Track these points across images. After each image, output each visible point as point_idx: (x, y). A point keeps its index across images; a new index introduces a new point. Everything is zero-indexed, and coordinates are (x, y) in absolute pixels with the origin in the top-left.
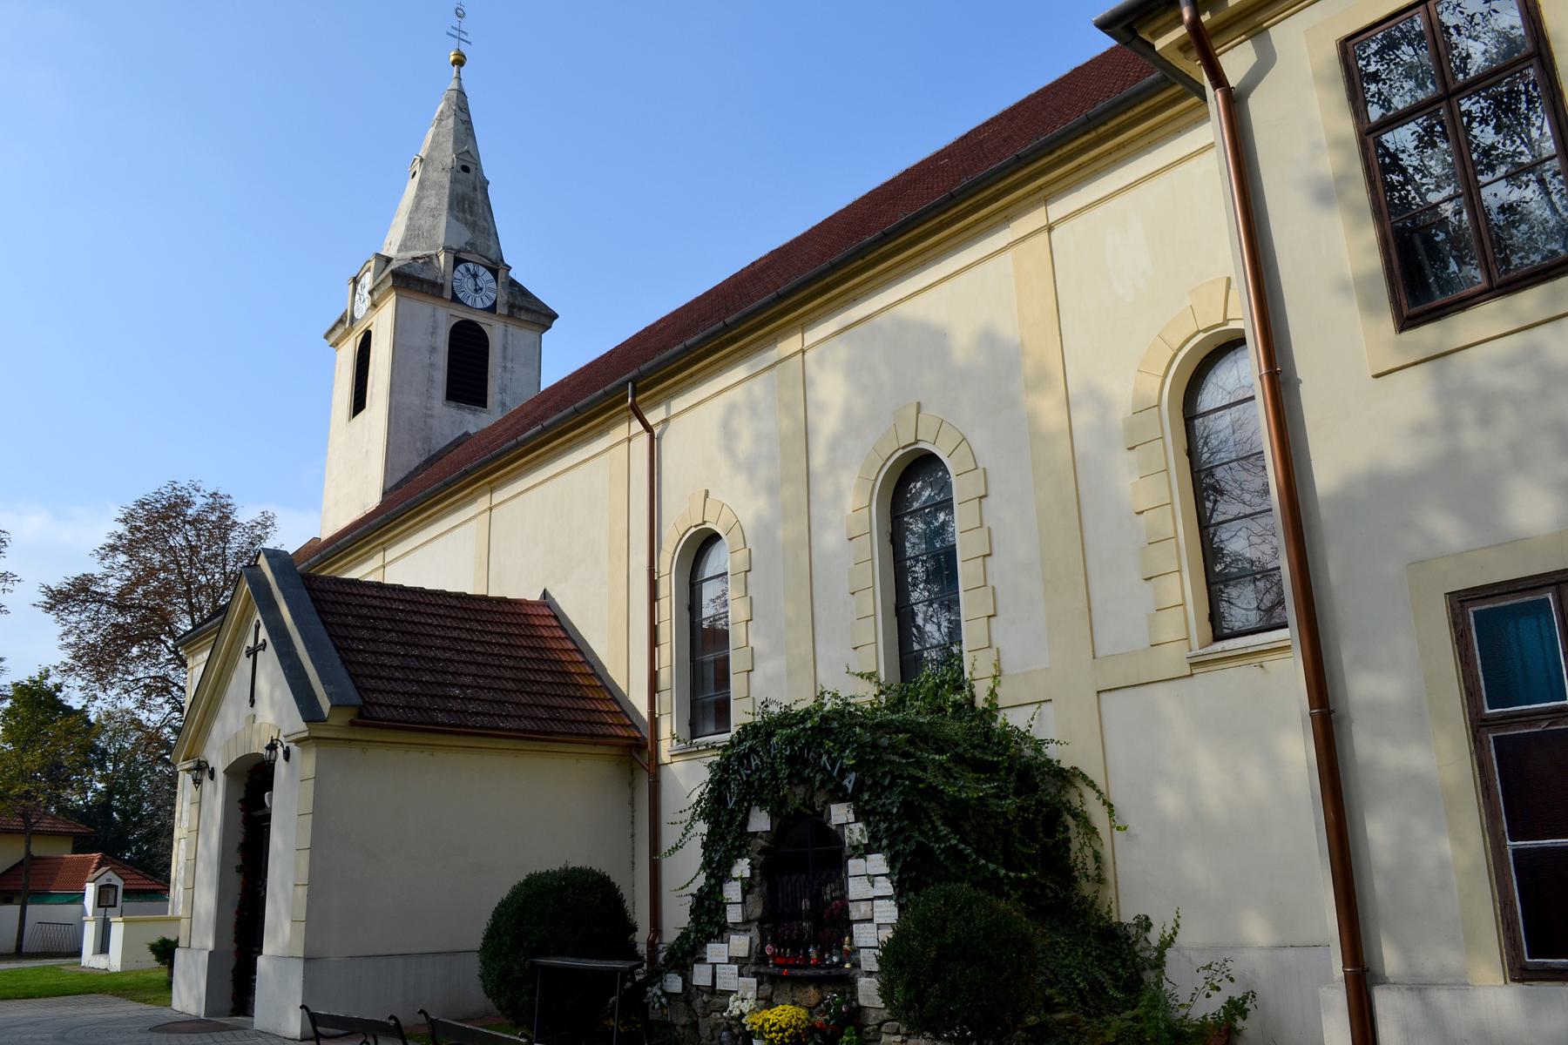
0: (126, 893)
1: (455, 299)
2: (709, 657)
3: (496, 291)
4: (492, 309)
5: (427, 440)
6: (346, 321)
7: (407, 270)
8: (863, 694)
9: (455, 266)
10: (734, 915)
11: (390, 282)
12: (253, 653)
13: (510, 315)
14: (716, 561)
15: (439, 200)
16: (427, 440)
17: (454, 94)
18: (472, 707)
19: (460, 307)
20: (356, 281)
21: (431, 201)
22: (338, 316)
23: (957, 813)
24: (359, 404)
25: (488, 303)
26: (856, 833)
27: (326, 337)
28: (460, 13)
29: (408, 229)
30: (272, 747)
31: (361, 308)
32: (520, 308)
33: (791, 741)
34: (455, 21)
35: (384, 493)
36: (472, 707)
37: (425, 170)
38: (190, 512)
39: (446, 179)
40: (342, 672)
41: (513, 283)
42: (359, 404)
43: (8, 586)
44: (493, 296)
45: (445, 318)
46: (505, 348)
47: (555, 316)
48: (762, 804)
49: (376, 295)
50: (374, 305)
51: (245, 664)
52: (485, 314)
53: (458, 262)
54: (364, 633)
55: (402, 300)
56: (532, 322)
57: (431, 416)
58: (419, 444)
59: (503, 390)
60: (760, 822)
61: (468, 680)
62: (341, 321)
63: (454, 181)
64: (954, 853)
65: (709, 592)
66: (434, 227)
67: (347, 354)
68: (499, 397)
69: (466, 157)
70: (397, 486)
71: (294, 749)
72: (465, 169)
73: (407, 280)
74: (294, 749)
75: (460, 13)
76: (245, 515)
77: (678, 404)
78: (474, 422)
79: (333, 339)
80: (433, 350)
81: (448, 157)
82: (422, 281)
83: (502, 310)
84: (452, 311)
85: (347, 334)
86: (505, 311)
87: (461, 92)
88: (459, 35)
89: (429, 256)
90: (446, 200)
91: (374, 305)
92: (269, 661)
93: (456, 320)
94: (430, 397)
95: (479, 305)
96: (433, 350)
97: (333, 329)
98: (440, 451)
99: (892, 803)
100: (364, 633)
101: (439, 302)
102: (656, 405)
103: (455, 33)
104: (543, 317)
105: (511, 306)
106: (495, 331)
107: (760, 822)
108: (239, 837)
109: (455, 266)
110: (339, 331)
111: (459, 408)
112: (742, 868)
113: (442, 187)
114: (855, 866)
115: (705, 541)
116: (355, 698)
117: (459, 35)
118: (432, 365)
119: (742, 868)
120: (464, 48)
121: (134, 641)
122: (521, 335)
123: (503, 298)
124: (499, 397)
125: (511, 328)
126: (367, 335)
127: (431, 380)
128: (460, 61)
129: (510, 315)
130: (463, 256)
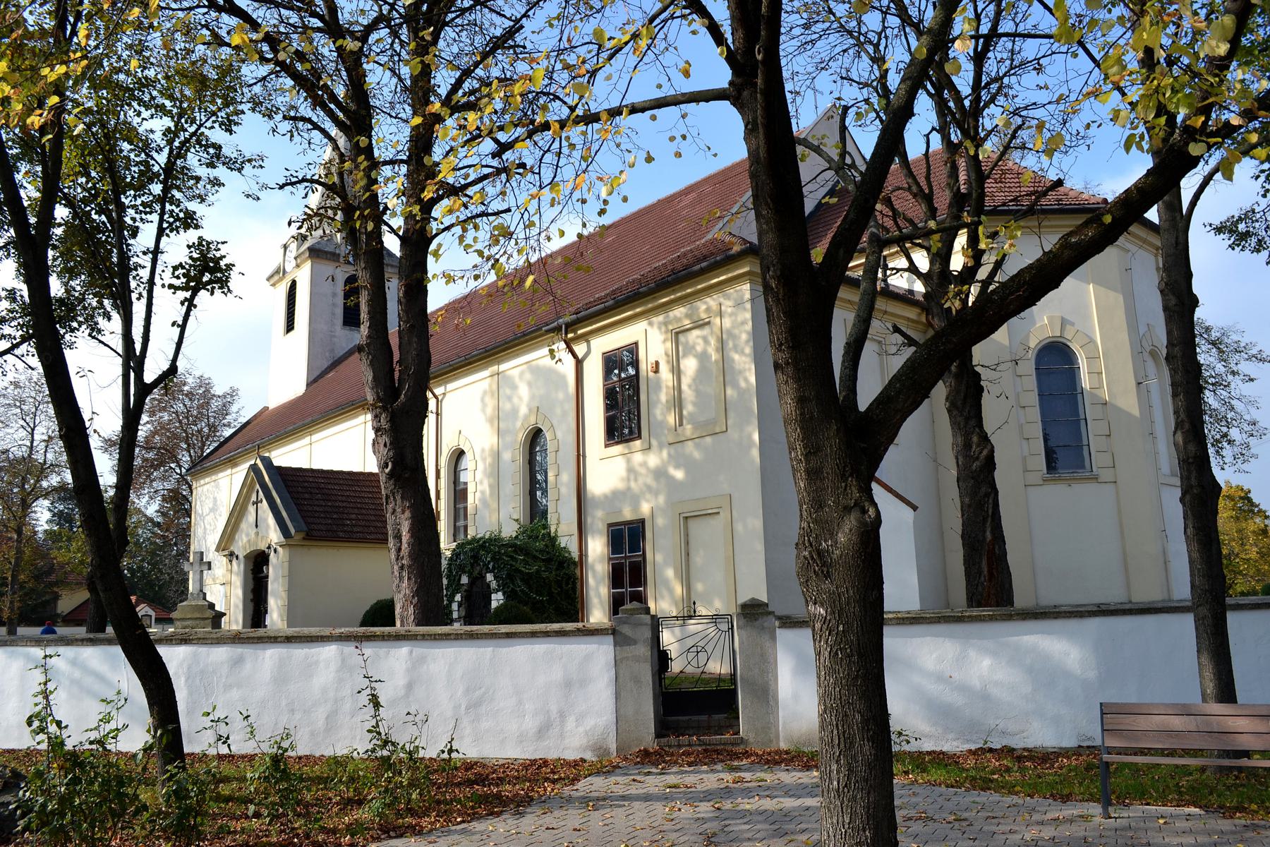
0: (156, 619)
2: (461, 506)
5: (332, 351)
6: (279, 272)
7: (317, 247)
8: (509, 531)
10: (455, 615)
12: (256, 503)
14: (467, 462)
16: (332, 351)
18: (355, 529)
20: (285, 247)
23: (527, 579)
24: (290, 326)
26: (494, 585)
30: (269, 548)
31: (290, 266)
33: (472, 550)
36: (355, 529)
38: (186, 388)
40: (299, 517)
42: (290, 326)
48: (465, 572)
50: (298, 266)
51: (252, 509)
54: (307, 496)
60: (465, 580)
61: (353, 516)
62: (277, 272)
64: (522, 591)
65: (462, 474)
67: (283, 288)
70: (315, 381)
71: (279, 549)
74: (279, 549)
76: (218, 390)
77: (450, 386)
79: (272, 281)
82: (326, 252)
85: (281, 280)
91: (298, 266)
92: (265, 504)
96: (334, 295)
99: (504, 574)
100: (307, 496)
102: (440, 385)
107: (465, 580)
108: (251, 586)
110: (276, 278)
112: (458, 597)
114: (493, 596)
115: (459, 454)
116: (305, 528)
118: (334, 305)
119: (458, 597)
121: (156, 468)
126: (294, 284)
127: (333, 314)
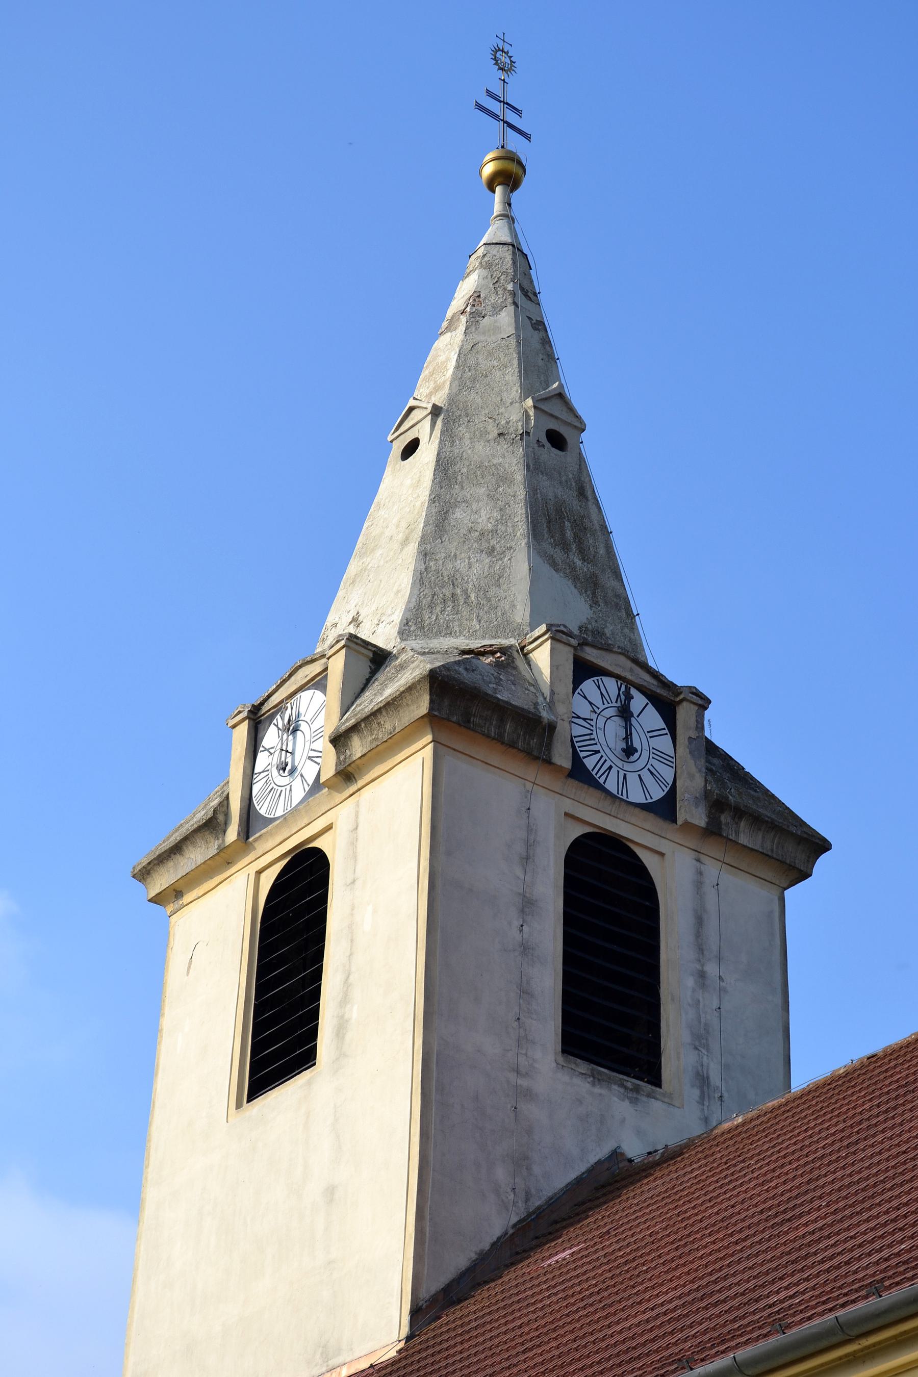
1: (579, 773)
3: (671, 761)
4: (665, 808)
9: (577, 682)
11: (422, 705)
13: (712, 831)
15: (502, 506)
16: (521, 1162)
17: (506, 254)
19: (590, 796)
21: (477, 512)
22: (201, 816)
25: (657, 793)
27: (144, 874)
28: (503, 61)
29: (421, 579)
32: (739, 813)
34: (492, 78)
35: (416, 1312)
37: (448, 436)
39: (513, 461)
41: (711, 749)
43: (533, 1191)
44: (668, 774)
45: (554, 819)
46: (699, 922)
47: (821, 846)
49: (358, 747)
52: (651, 821)
53: (583, 671)
55: (450, 760)
56: (765, 857)
57: (528, 1095)
58: (501, 1174)
59: (700, 1040)
62: (213, 824)
63: (533, 468)
66: (498, 579)
67: (217, 930)
68: (689, 1059)
69: (555, 408)
72: (556, 440)
73: (469, 707)
75: (503, 61)
78: (635, 1125)
79: (162, 881)
80: (527, 905)
81: (517, 410)
82: (503, 710)
83: (692, 812)
84: (568, 805)
85: (224, 861)
86: (699, 818)
87: (516, 249)
88: (501, 111)
89: (504, 650)
90: (519, 512)
91: (347, 775)
93: (578, 831)
94: (523, 1041)
95: (636, 795)
97: (177, 849)
98: (553, 1202)
101: (531, 772)
103: (496, 107)
104: (793, 848)
105: (716, 806)
106: (676, 870)
109: (577, 682)
110: (196, 856)
111: (596, 1079)
113: (505, 479)
117: (501, 111)
120: (515, 143)
122: (738, 891)
123: (692, 784)
124: (689, 1059)
125: (712, 869)
127: (525, 992)
128: (509, 177)
129: (712, 831)
130: (592, 655)
